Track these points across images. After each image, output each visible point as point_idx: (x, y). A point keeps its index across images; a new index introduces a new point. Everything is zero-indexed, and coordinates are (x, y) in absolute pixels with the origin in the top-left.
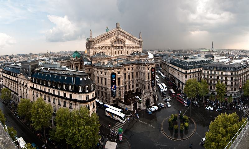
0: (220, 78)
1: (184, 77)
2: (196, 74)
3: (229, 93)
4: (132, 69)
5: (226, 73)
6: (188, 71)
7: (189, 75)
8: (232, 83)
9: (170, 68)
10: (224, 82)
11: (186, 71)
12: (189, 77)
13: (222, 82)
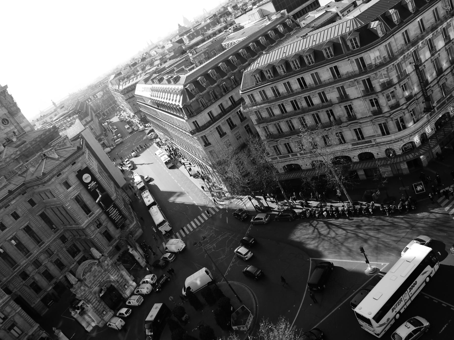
4: (15, 216)
8: (375, 103)
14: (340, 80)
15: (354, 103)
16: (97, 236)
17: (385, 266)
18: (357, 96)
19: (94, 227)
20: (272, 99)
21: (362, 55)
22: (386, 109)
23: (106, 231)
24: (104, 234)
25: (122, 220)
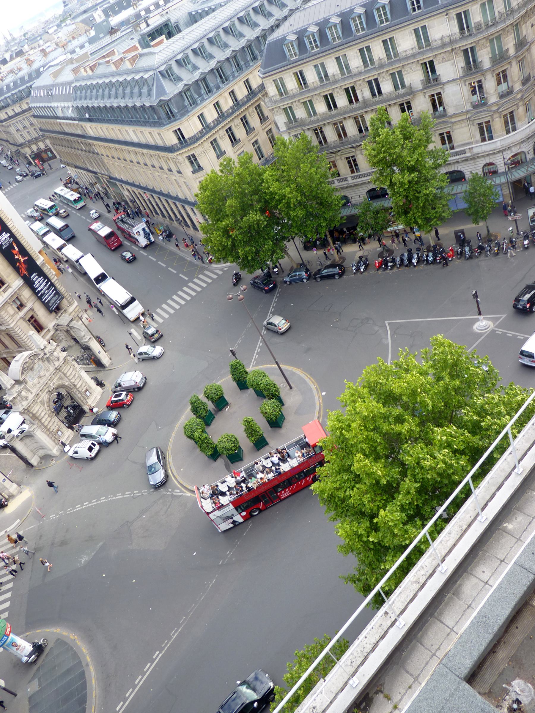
0: (387, 87)
1: (187, 169)
2: (245, 121)
3: (474, 158)
5: (421, 35)
6: (191, 126)
7: (208, 145)
8: (478, 89)
9: (99, 147)
10: (421, 105)
11: (179, 133)
12: (212, 154)
13: (406, 107)
14: (396, 61)
15: (446, 90)
16: (18, 323)
17: (501, 319)
18: (452, 76)
19: (13, 309)
20: (295, 91)
21: (425, 23)
22: (493, 99)
23: (32, 317)
24: (29, 321)
25: (55, 298)
